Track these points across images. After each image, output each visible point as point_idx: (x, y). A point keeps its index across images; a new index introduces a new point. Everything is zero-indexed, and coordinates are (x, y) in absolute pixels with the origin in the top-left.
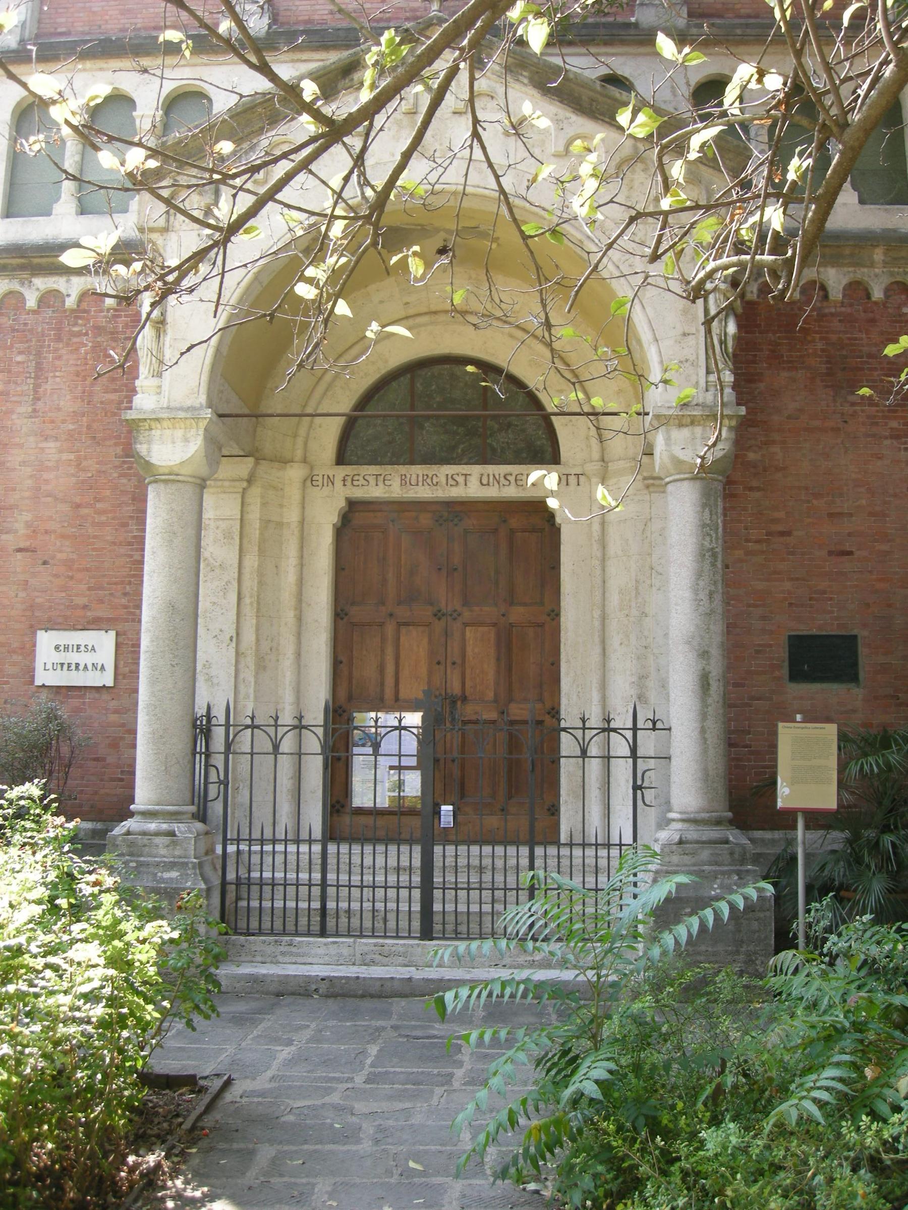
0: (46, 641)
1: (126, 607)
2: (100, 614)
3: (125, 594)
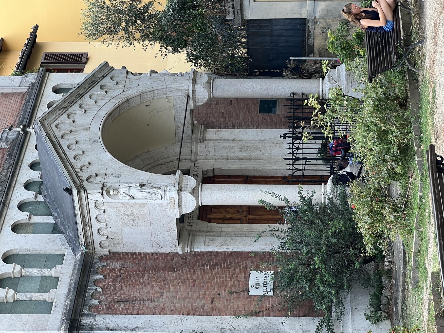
0: (253, 292)
1: (240, 269)
2: (243, 277)
3: (234, 270)
